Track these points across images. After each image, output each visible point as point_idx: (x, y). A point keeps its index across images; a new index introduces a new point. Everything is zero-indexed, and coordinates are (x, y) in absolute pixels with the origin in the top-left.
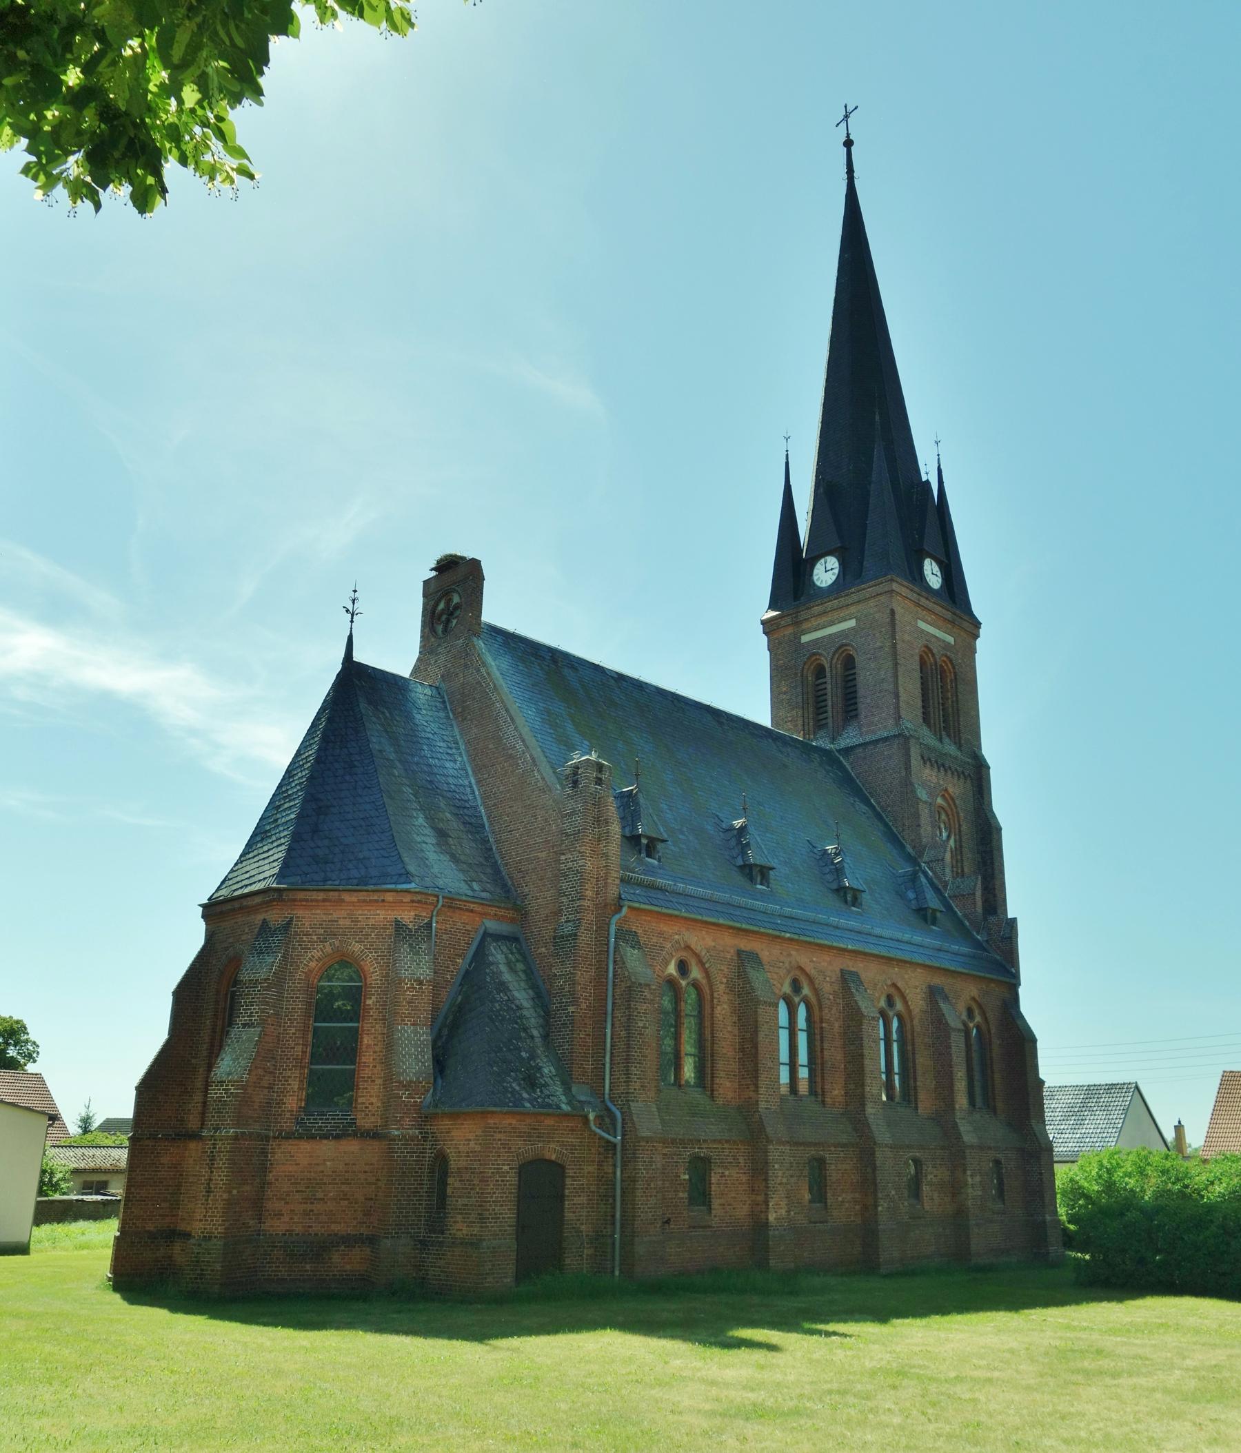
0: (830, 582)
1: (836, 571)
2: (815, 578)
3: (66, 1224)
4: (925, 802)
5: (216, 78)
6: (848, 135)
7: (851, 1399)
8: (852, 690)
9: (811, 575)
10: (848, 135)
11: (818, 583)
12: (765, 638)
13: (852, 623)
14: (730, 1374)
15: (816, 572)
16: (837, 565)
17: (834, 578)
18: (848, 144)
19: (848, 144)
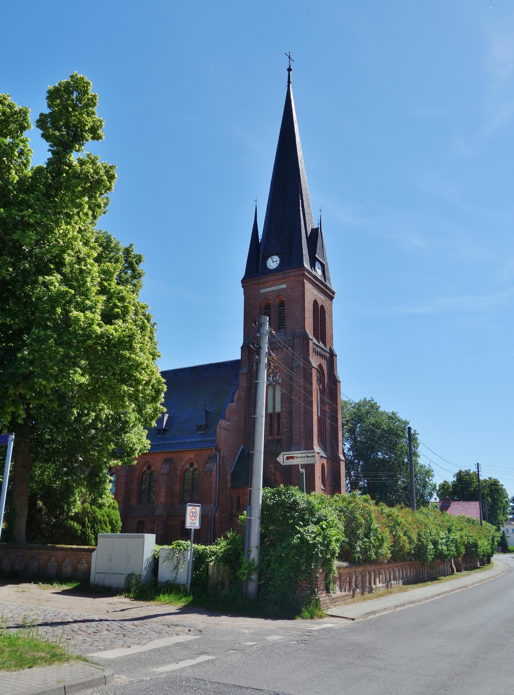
0: (275, 267)
1: (278, 262)
2: (268, 265)
3: (227, 617)
4: (315, 369)
5: (316, 628)
6: (290, 66)
7: (154, 633)
8: (283, 321)
9: (266, 264)
10: (290, 66)
11: (269, 267)
12: (242, 289)
13: (284, 286)
14: (118, 615)
15: (268, 262)
16: (278, 260)
17: (277, 265)
18: (289, 70)
19: (289, 70)
